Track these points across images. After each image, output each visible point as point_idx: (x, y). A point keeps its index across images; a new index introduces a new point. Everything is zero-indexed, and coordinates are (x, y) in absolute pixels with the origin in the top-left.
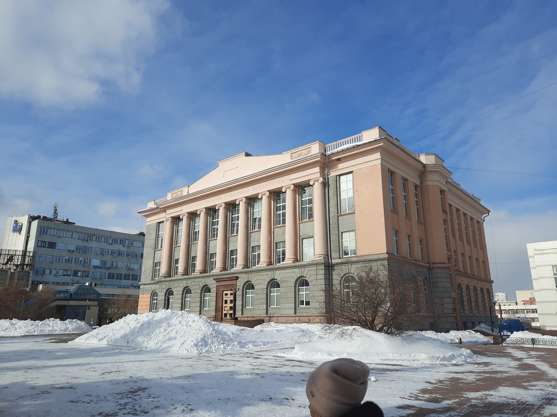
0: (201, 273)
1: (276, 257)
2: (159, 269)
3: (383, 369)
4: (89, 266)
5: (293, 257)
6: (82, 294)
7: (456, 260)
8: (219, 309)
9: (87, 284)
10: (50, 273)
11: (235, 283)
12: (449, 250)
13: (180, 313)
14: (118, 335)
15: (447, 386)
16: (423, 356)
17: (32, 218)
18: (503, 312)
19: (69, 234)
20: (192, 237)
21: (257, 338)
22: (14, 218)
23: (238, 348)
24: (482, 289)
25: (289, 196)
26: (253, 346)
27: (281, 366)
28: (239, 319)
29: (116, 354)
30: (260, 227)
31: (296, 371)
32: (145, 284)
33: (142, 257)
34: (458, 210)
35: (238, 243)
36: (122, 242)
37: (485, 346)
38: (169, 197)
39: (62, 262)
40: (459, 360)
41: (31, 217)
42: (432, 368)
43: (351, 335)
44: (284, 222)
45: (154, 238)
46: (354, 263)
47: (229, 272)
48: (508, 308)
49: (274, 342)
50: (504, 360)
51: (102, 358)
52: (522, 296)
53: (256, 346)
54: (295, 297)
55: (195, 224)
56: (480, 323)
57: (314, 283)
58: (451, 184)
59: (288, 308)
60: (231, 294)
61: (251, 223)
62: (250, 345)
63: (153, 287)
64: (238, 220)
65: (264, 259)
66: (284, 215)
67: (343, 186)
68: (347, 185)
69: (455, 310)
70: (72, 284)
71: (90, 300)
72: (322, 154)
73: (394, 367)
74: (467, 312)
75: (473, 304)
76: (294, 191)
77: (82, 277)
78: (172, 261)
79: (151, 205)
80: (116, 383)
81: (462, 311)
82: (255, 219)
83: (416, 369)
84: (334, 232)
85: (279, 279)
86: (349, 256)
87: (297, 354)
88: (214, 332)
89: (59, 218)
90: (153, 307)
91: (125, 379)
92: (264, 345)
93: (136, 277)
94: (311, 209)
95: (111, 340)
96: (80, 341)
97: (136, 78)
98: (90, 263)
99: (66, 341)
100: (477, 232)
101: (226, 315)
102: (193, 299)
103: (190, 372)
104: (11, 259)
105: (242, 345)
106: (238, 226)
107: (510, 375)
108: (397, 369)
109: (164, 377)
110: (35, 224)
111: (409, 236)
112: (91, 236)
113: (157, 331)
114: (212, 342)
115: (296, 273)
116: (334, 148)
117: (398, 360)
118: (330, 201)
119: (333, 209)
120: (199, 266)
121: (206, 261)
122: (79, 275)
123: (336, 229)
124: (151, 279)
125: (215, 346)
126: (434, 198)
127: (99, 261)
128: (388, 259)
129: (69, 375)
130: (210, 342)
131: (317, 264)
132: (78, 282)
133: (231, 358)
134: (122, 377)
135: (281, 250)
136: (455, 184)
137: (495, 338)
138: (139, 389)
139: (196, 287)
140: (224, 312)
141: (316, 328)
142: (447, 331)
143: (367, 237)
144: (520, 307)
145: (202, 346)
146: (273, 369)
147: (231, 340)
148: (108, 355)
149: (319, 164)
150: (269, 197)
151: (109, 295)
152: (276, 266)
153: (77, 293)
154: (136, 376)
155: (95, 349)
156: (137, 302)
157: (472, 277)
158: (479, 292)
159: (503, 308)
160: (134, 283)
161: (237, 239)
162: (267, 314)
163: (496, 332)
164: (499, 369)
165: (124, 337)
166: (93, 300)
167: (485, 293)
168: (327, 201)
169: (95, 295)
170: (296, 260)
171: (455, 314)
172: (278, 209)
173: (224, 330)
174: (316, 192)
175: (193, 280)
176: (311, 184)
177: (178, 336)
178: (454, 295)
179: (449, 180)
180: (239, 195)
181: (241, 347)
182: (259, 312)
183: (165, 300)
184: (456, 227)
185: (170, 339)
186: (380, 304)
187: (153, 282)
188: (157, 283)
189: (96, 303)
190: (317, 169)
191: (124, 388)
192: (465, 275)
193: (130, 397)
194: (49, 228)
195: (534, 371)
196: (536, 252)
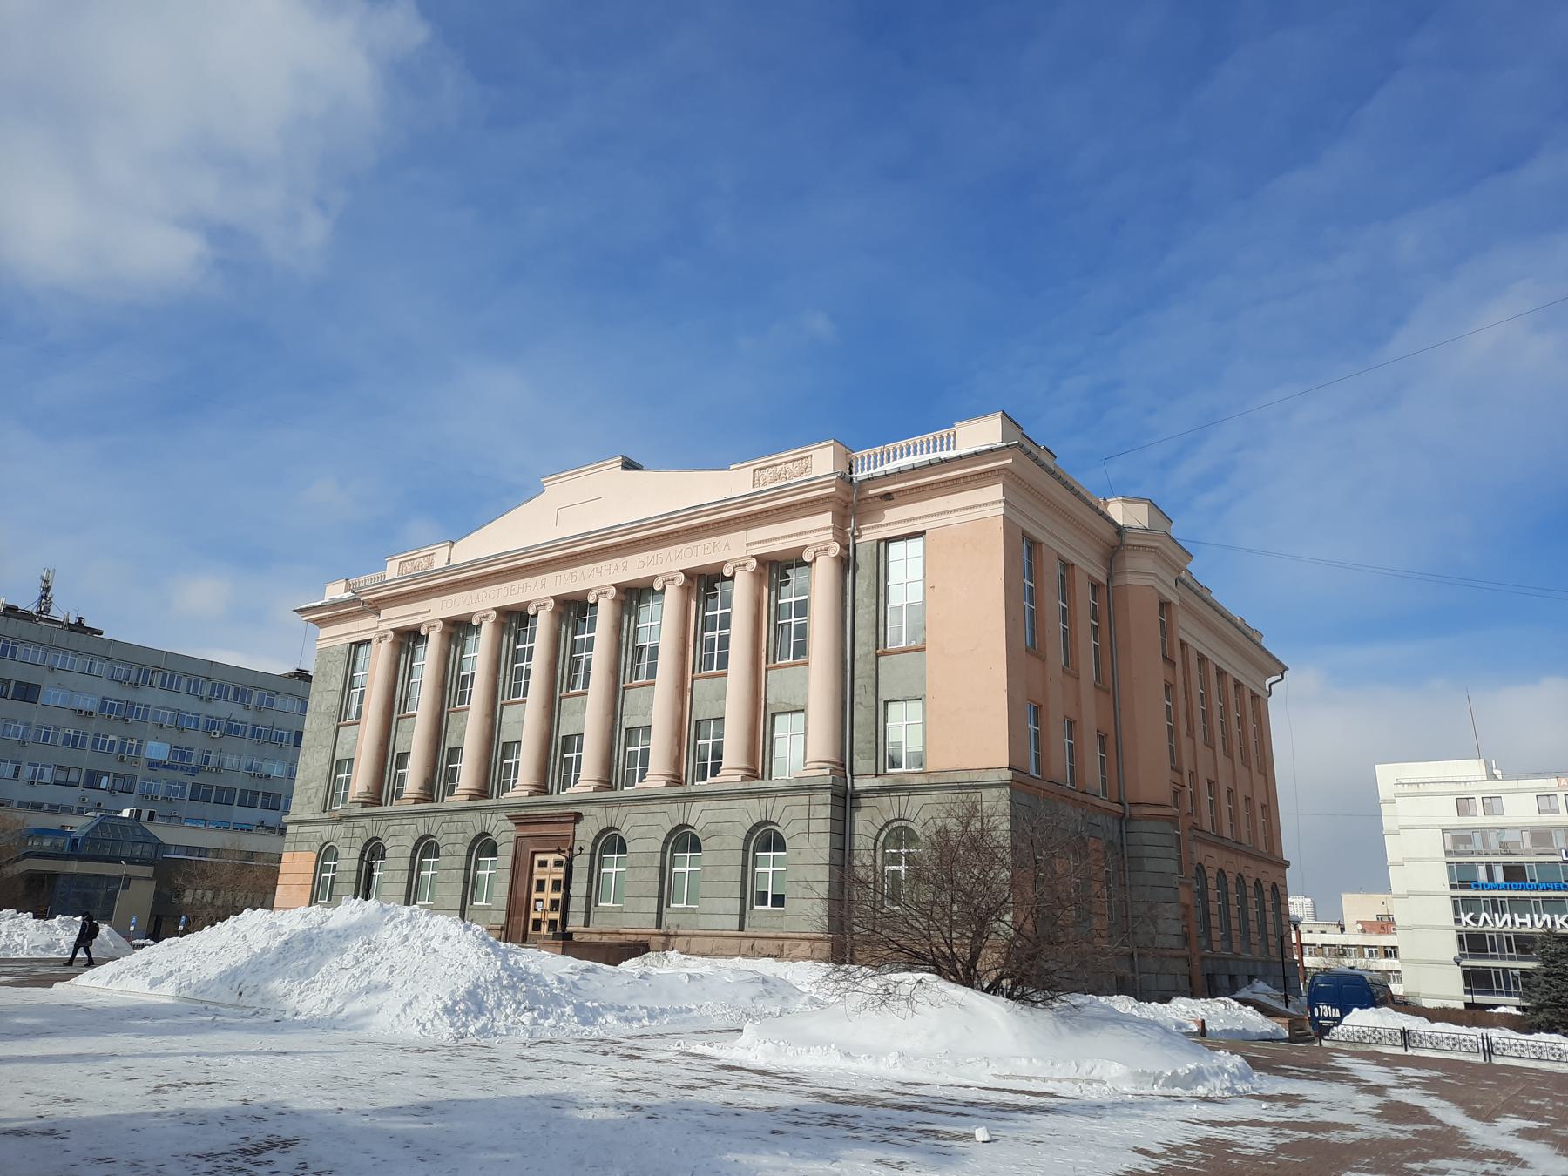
0: (472, 797)
1: (694, 759)
2: (348, 780)
3: (1005, 1104)
4: (136, 759)
5: (744, 765)
6: (106, 841)
7: (1195, 797)
8: (517, 905)
9: (126, 813)
10: (16, 775)
11: (570, 832)
12: (1177, 769)
13: (406, 910)
14: (212, 971)
15: (1197, 1164)
16: (1115, 1070)
18: (1306, 950)
19: (81, 663)
20: (451, 689)
21: (631, 998)
23: (574, 1024)
24: (1258, 883)
25: (741, 591)
26: (620, 1019)
27: (705, 1084)
28: (576, 938)
29: (201, 1028)
30: (652, 673)
31: (752, 1101)
32: (301, 823)
33: (298, 743)
34: (1202, 659)
35: (587, 717)
36: (241, 695)
37: (1269, 1046)
38: (392, 570)
39: (54, 744)
40: (1215, 1086)
42: (1141, 1105)
43: (909, 999)
44: (723, 663)
45: (339, 687)
46: (915, 789)
47: (554, 797)
48: (1319, 939)
49: (681, 1011)
50: (1337, 1091)
51: (157, 1039)
52: (1358, 907)
53: (627, 1020)
54: (744, 882)
55: (462, 653)
56: (1251, 978)
57: (801, 841)
58: (1187, 585)
59: (721, 913)
60: (558, 864)
61: (627, 659)
62: (610, 1018)
63: (326, 831)
64: (590, 649)
65: (658, 765)
66: (724, 641)
67: (896, 573)
68: (906, 570)
69: (1186, 938)
70: (81, 812)
71: (130, 861)
72: (842, 477)
73: (1035, 1101)
74: (1217, 946)
75: (1235, 924)
76: (758, 576)
77: (111, 790)
78: (388, 758)
80: (201, 1120)
81: (1204, 942)
82: (641, 649)
83: (1096, 1109)
84: (863, 697)
85: (699, 827)
86: (904, 769)
87: (751, 1049)
88: (504, 975)
89: (55, 613)
90: (321, 892)
91: (227, 1110)
92: (651, 1017)
93: (277, 801)
94: (802, 631)
95: (190, 985)
96: (93, 983)
97: (316, 230)
98: (138, 750)
99: (47, 982)
100: (1251, 725)
101: (537, 924)
102: (444, 872)
103: (430, 1093)
105: (587, 1016)
106: (588, 667)
107: (1366, 1136)
108: (1045, 1106)
109: (350, 1106)
111: (1071, 724)
112: (147, 672)
113: (334, 963)
114: (499, 1005)
115: (750, 812)
116: (875, 464)
117: (1045, 1080)
118: (859, 612)
119: (864, 635)
120: (467, 774)
121: (489, 762)
122: (103, 786)
123: (872, 690)
124: (321, 807)
125: (507, 1016)
126: (1141, 624)
127: (167, 746)
128: (1013, 785)
129: (47, 1090)
130: (491, 1003)
132: (98, 807)
133: (554, 1056)
134: (217, 1101)
135: (710, 741)
136: (1197, 588)
137: (1294, 1024)
138: (271, 1144)
139: (454, 838)
140: (533, 916)
141: (806, 974)
142: (1165, 999)
143: (956, 720)
144: (1353, 938)
145: (466, 1013)
146: (684, 1092)
147: (556, 1000)
148: (178, 1030)
149: (831, 506)
150: (686, 589)
151: (189, 849)
152: (693, 789)
153: (91, 837)
154: (262, 1100)
155: (138, 1008)
156: (273, 874)
157: (1234, 848)
158: (1251, 892)
159: (1306, 939)
160: (270, 817)
161: (584, 705)
162: (659, 926)
163: (1295, 1008)
164: (1330, 1117)
165: (231, 977)
166: (141, 862)
167: (1268, 895)
168: (849, 610)
169: (147, 848)
170: (752, 773)
171: (1186, 953)
172: (707, 624)
173: (533, 969)
174: (820, 582)
175: (447, 817)
176: (807, 558)
177: (397, 983)
178: (1185, 896)
179: (1183, 574)
180: (599, 579)
181: (585, 1022)
182: (637, 919)
183: (359, 871)
184: (1198, 707)
185: (371, 989)
186: (996, 911)
187: (326, 816)
188: (339, 821)
189: (148, 871)
190: (826, 519)
191: (224, 1140)
192: (1216, 841)
193: (240, 1170)
194: (20, 640)
195: (1428, 1127)
196: (1400, 789)
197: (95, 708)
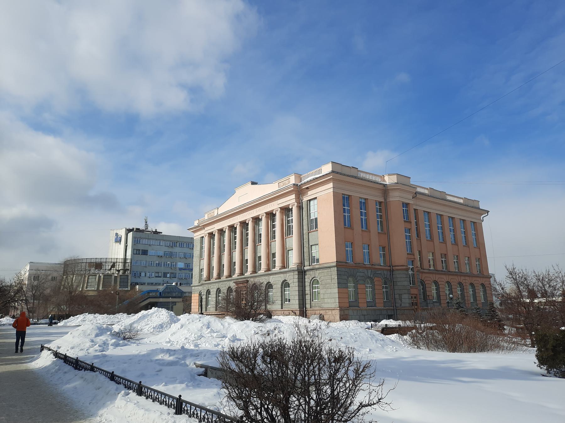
4: (176, 268)
9: (174, 284)
17: (129, 231)
19: (157, 243)
22: (115, 232)
32: (195, 286)
38: (206, 218)
41: (127, 230)
54: (282, 296)
61: (257, 238)
71: (172, 297)
77: (170, 277)
79: (196, 223)
84: (306, 245)
89: (149, 229)
104: (113, 266)
110: (130, 235)
120: (226, 273)
127: (183, 264)
131: (293, 271)
170: (283, 267)
175: (222, 283)
189: (181, 300)
190: (293, 196)
194: (141, 238)
197: (163, 255)
